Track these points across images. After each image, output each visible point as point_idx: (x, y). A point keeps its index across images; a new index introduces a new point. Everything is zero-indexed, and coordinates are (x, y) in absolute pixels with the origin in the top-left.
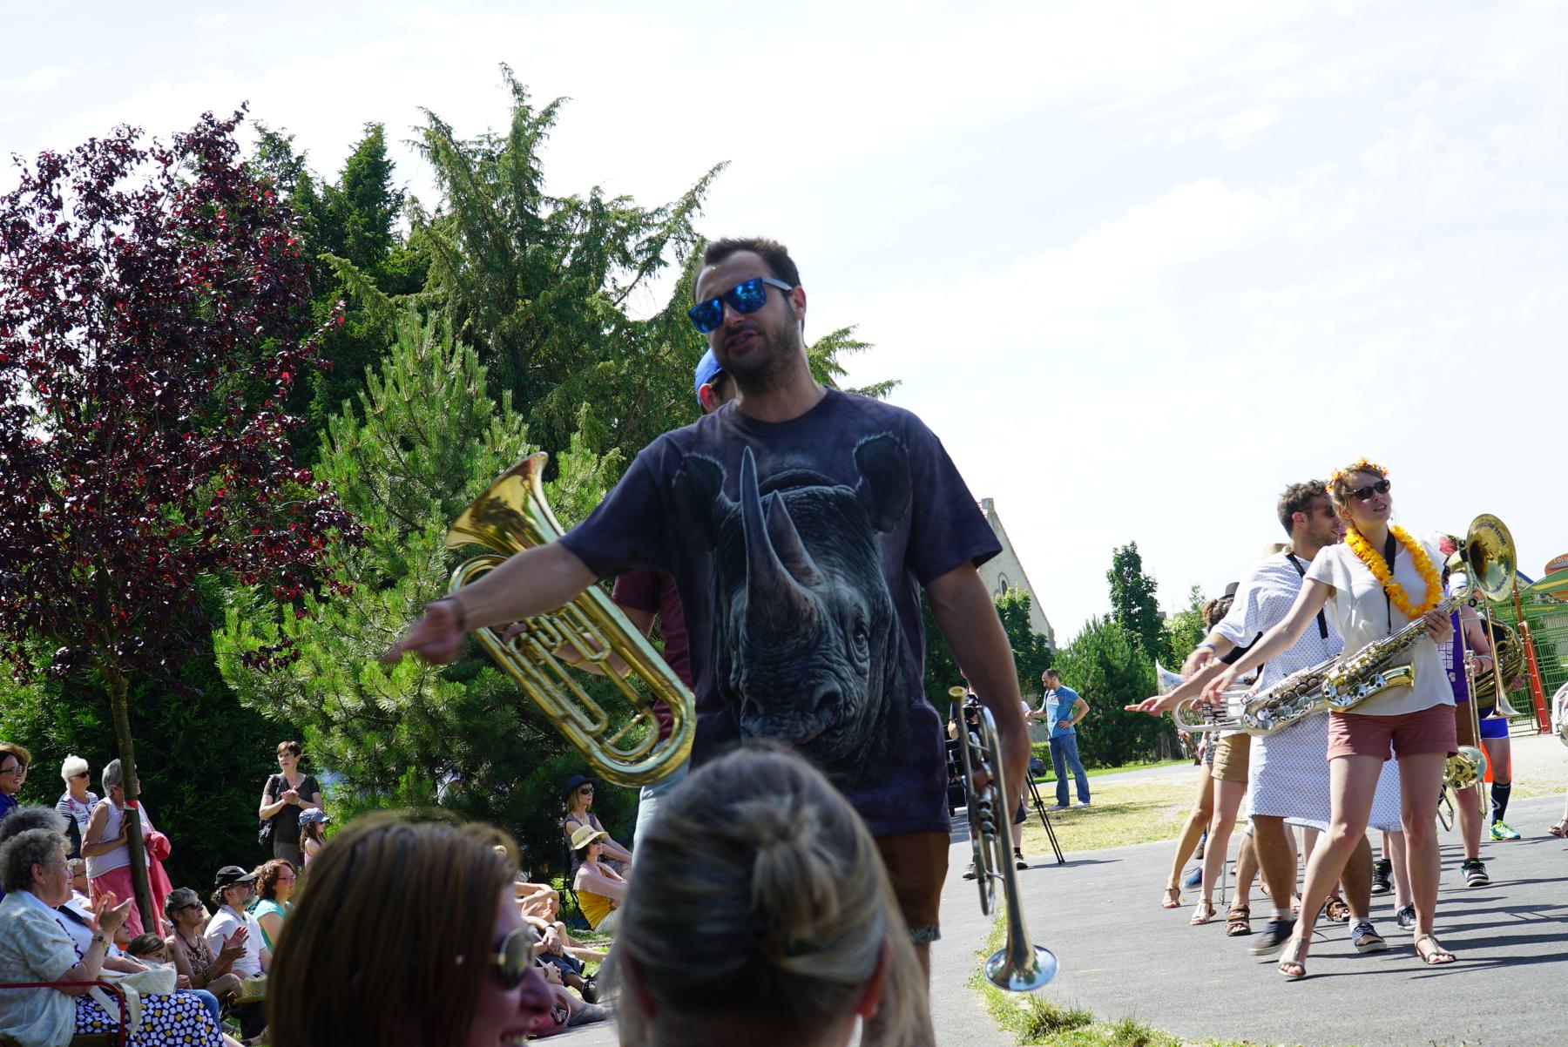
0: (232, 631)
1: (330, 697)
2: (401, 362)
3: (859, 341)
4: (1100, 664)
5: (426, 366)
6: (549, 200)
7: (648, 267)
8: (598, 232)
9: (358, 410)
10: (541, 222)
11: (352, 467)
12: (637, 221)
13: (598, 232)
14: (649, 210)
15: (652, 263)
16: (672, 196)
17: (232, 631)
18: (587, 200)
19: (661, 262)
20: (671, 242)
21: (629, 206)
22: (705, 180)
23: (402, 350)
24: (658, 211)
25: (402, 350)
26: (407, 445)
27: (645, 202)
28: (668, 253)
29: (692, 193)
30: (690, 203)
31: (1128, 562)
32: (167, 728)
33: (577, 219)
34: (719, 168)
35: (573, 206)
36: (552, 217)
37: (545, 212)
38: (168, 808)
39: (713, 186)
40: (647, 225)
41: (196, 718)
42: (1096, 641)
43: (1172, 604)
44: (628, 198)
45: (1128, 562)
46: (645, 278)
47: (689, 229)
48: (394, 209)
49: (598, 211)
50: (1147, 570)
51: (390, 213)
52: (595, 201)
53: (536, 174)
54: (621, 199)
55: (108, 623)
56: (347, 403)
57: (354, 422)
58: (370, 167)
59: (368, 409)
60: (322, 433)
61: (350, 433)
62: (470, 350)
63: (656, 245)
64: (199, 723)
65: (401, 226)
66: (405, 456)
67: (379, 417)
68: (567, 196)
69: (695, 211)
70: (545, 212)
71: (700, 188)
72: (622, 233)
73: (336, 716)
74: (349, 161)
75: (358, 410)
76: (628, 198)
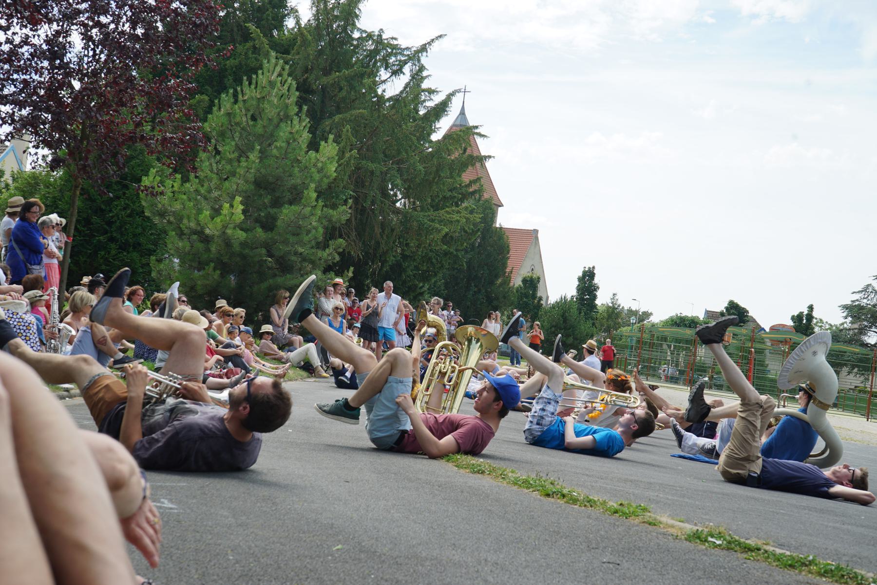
0: (151, 178)
1: (185, 221)
2: (262, 78)
3: (483, 133)
4: (562, 316)
5: (272, 84)
6: (359, 29)
7: (395, 73)
8: (376, 52)
9: (235, 96)
10: (353, 39)
11: (225, 120)
12: (396, 49)
13: (376, 52)
14: (403, 47)
15: (396, 72)
16: (415, 43)
17: (151, 178)
18: (377, 33)
19: (402, 72)
20: (410, 64)
21: (395, 42)
22: (433, 40)
23: (263, 74)
24: (407, 49)
25: (263, 74)
26: (254, 118)
27: (403, 43)
28: (407, 69)
29: (425, 45)
30: (424, 49)
31: (588, 276)
32: (112, 217)
33: (370, 42)
34: (440, 36)
35: (370, 36)
36: (359, 38)
37: (356, 35)
38: (103, 253)
39: (436, 44)
40: (400, 54)
41: (127, 216)
42: (563, 306)
43: (602, 299)
44: (396, 39)
45: (588, 276)
46: (394, 77)
47: (419, 61)
48: (288, 14)
49: (379, 41)
50: (596, 280)
51: (286, 15)
52: (380, 36)
53: (357, 16)
54: (392, 38)
55: (80, 153)
56: (231, 91)
57: (232, 100)
58: (441, 109)
59: (240, 96)
60: (216, 101)
61: (228, 106)
62: (294, 83)
63: (403, 63)
64: (128, 219)
65: (290, 23)
66: (251, 123)
67: (244, 101)
68: (369, 30)
69: (424, 54)
70: (356, 35)
71: (429, 43)
72: (390, 55)
73: (186, 231)
74: (710, 314)
75: (235, 96)
76: (396, 39)
